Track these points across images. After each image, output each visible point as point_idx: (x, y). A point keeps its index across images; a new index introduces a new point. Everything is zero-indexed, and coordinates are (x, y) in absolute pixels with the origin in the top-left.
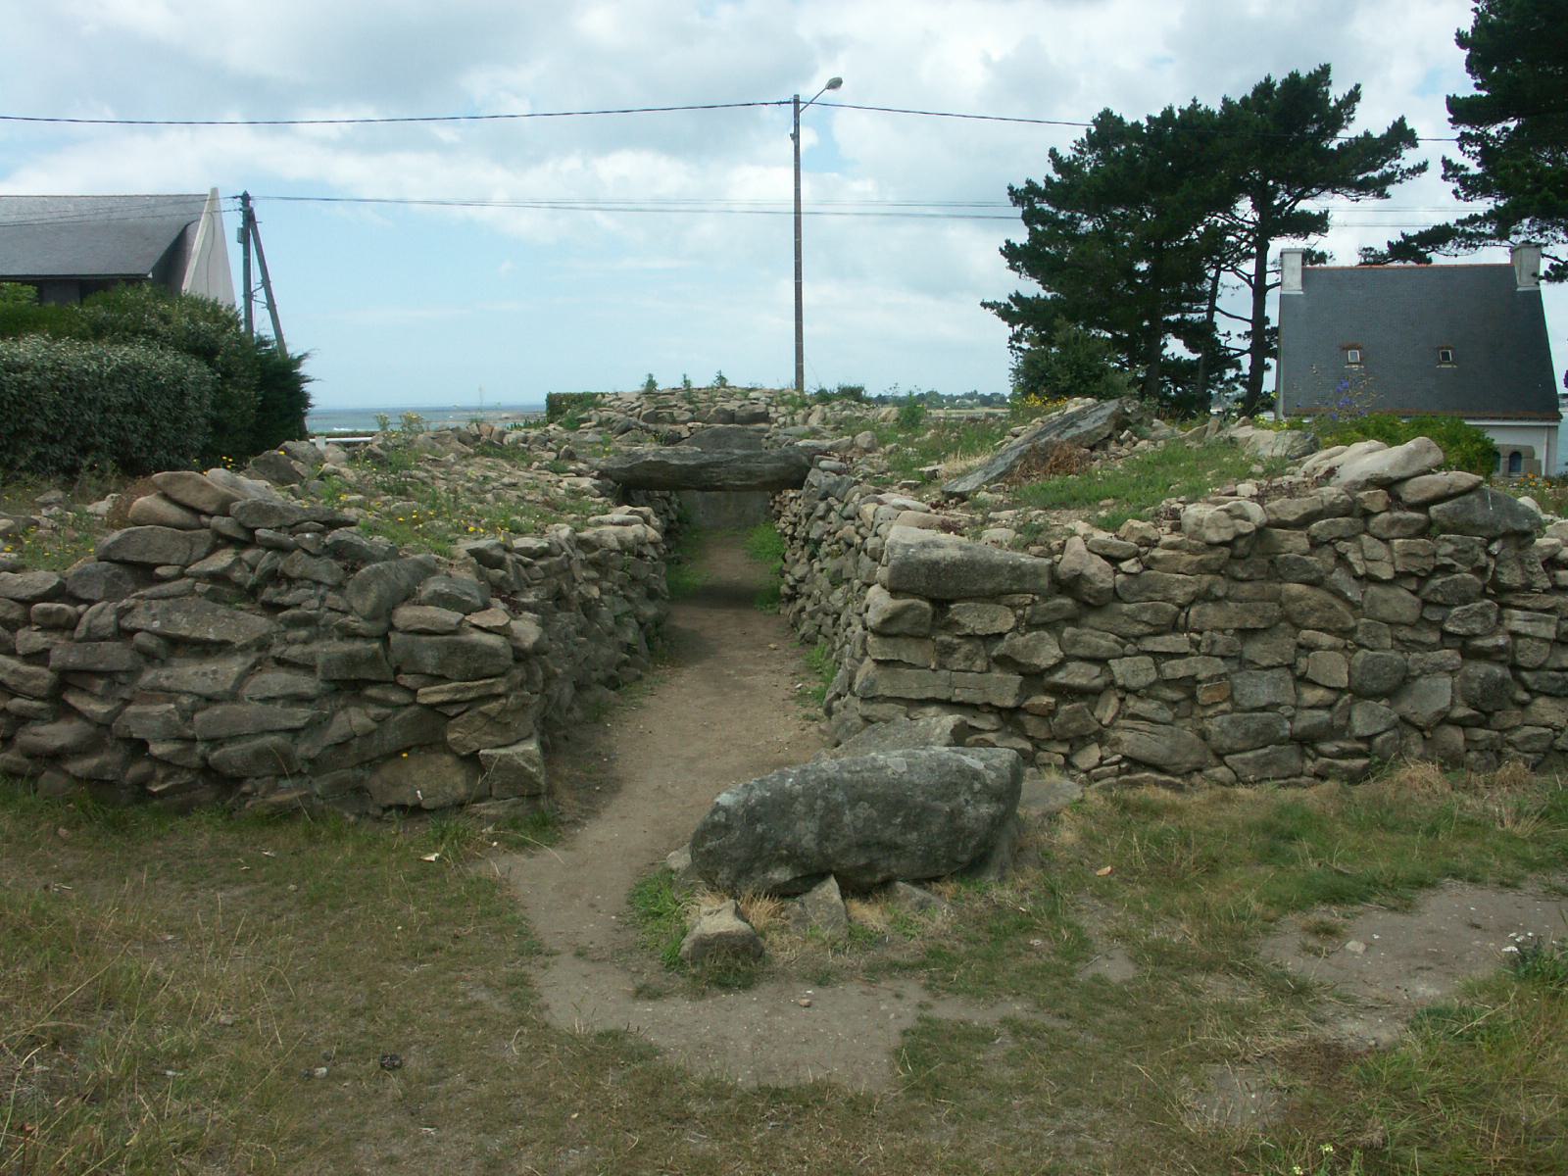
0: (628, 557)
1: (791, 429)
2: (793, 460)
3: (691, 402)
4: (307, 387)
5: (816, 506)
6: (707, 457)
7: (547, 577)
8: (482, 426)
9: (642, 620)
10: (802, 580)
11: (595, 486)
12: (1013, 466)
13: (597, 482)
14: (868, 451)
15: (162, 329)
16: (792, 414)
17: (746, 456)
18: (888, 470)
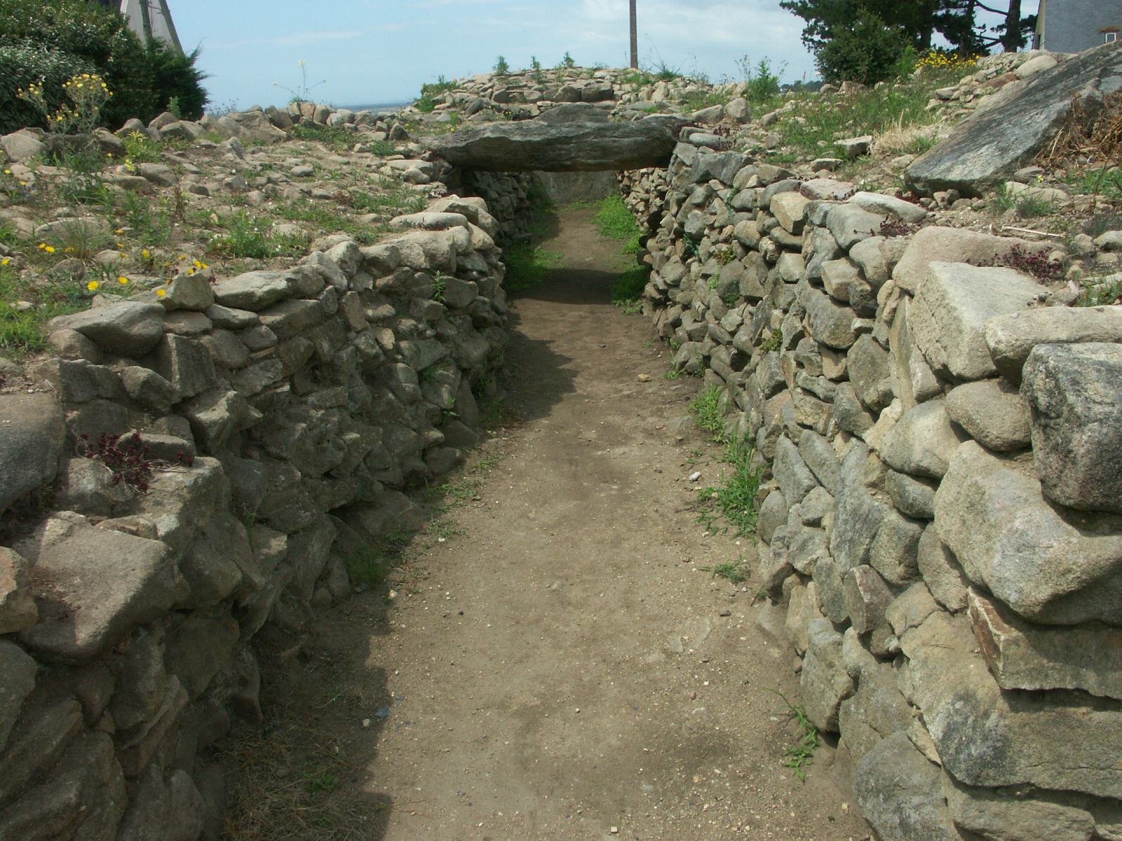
0: (440, 277)
1: (637, 105)
2: (656, 134)
3: (540, 82)
4: (202, 84)
5: (692, 190)
6: (553, 131)
7: (280, 341)
8: (303, 106)
9: (465, 365)
10: (676, 284)
11: (423, 170)
12: (1047, 138)
13: (428, 164)
14: (741, 121)
15: (47, 29)
16: (636, 91)
17: (600, 129)
18: (782, 144)
